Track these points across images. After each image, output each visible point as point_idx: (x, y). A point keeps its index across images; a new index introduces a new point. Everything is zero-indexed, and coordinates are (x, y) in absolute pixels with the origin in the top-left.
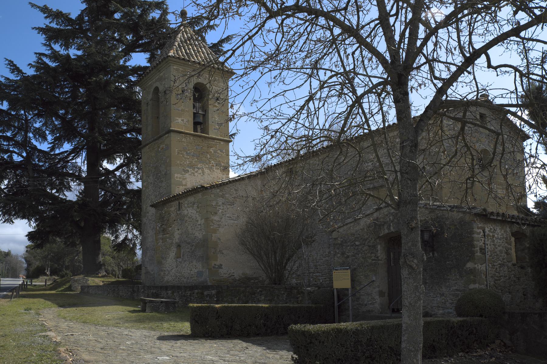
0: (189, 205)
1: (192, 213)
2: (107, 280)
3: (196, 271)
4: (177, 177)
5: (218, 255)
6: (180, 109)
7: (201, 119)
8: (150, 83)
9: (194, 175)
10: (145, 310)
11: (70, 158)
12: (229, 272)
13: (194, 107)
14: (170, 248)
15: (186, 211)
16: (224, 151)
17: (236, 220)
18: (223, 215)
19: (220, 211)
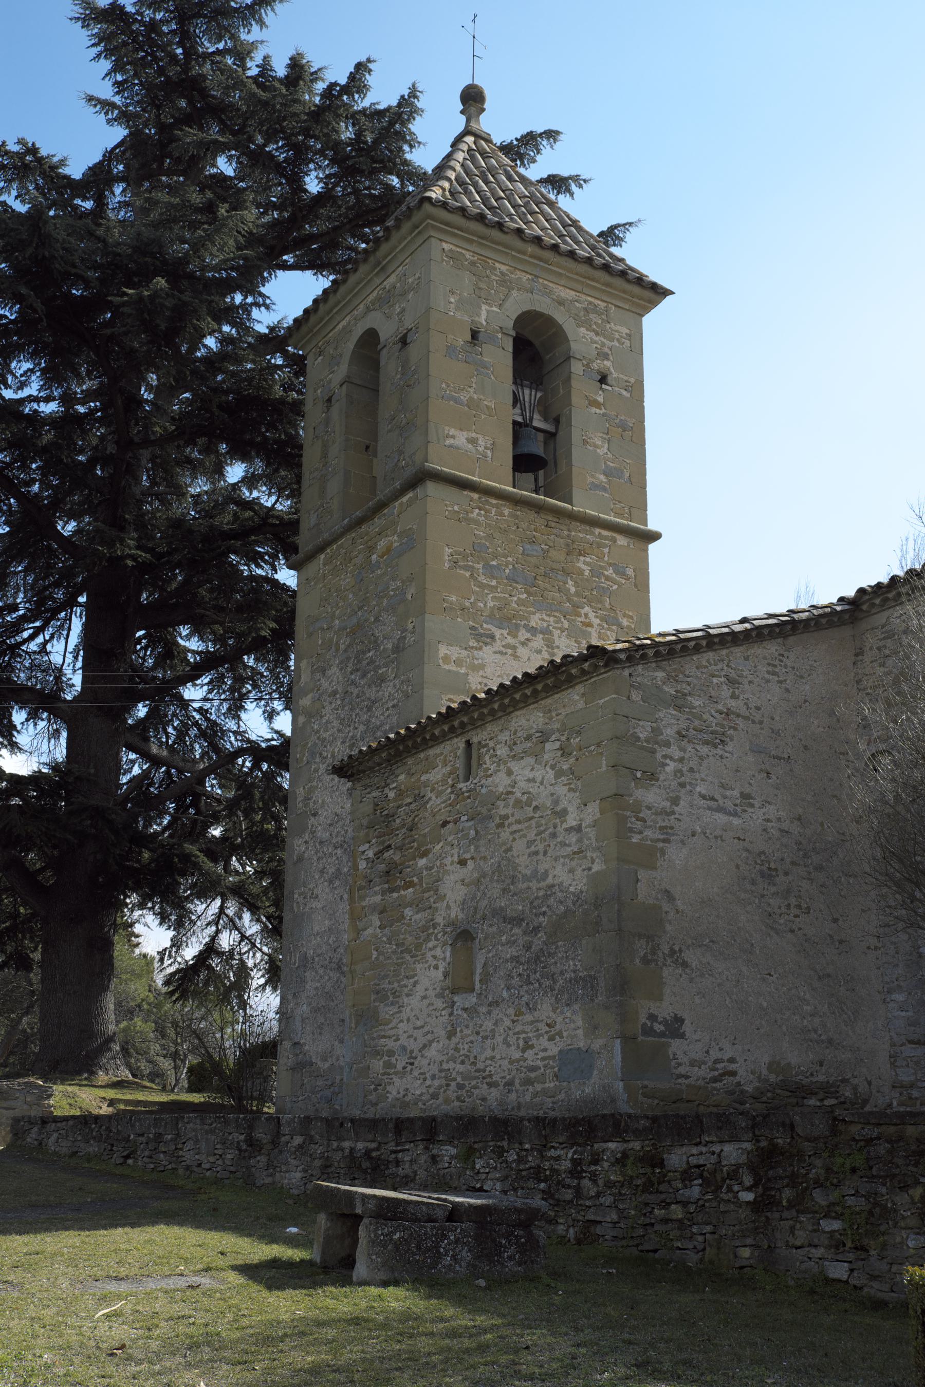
0: (518, 749)
1: (533, 780)
2: (128, 1097)
3: (554, 1050)
4: (446, 659)
5: (666, 972)
6: (464, 397)
7: (537, 448)
8: (344, 323)
9: (516, 657)
10: (349, 1262)
11: (26, 634)
12: (715, 1054)
13: (516, 400)
14: (418, 947)
15: (502, 775)
16: (630, 572)
17: (735, 814)
18: (682, 785)
19: (671, 767)
